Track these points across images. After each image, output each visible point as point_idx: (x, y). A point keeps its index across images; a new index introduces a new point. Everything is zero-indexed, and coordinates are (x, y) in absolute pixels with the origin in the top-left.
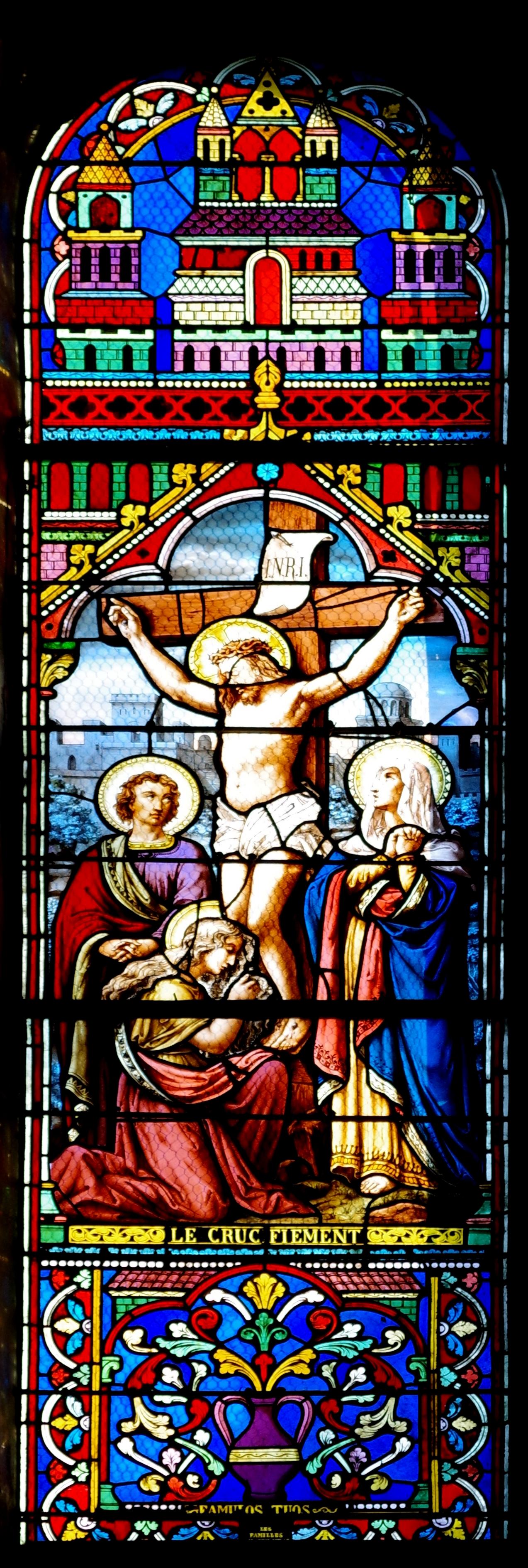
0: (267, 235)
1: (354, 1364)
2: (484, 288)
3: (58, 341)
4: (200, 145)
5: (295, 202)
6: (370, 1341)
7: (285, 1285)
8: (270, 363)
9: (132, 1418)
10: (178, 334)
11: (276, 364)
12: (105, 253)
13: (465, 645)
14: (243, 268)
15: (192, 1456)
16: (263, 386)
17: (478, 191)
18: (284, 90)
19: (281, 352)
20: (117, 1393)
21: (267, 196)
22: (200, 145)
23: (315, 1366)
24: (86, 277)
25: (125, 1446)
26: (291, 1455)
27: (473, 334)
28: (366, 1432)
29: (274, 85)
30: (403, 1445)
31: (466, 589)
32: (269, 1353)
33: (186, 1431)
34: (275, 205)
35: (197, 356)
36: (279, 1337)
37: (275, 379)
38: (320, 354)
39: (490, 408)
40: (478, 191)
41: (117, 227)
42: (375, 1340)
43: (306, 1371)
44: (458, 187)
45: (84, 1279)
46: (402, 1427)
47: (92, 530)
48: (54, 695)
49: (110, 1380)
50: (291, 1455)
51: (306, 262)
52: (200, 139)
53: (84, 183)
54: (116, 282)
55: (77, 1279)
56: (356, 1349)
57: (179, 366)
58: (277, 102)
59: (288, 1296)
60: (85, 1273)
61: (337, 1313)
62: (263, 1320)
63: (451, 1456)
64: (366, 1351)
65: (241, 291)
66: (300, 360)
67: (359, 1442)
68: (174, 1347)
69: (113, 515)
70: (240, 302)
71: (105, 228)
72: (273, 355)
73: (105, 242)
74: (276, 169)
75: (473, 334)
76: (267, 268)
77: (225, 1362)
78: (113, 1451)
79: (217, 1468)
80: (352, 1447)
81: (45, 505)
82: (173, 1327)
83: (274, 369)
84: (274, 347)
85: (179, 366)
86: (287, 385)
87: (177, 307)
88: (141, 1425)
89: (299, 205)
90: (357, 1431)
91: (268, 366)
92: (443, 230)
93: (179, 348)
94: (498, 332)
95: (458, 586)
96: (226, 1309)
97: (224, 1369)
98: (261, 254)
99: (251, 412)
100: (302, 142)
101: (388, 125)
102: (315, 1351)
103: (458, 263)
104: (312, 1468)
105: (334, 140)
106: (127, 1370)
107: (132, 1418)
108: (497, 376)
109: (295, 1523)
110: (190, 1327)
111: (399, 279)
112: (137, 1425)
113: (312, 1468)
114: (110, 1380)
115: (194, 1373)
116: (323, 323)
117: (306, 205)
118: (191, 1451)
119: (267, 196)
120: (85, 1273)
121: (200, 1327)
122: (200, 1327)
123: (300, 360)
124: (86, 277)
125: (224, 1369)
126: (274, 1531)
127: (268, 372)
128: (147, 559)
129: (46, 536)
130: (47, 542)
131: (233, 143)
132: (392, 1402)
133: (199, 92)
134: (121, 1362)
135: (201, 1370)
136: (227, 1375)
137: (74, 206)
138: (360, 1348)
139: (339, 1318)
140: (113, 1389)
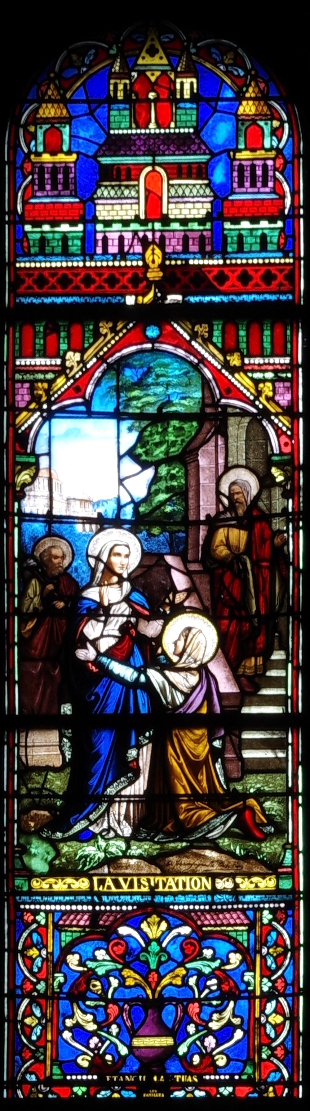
0: (154, 155)
1: (209, 977)
2: (286, 188)
3: (25, 234)
4: (112, 88)
5: (169, 127)
6: (219, 961)
7: (168, 922)
8: (155, 247)
9: (72, 1016)
10: (99, 227)
11: (158, 246)
12: (55, 169)
13: (276, 455)
14: (138, 180)
15: (108, 1042)
16: (151, 265)
17: (285, 117)
18: (162, 44)
19: (162, 238)
20: (64, 999)
21: (152, 125)
22: (112, 88)
23: (185, 979)
24: (42, 188)
25: (67, 1035)
26: (169, 1041)
27: (280, 224)
28: (214, 1026)
29: (156, 39)
30: (239, 1034)
31: (281, 417)
32: (157, 970)
33: (103, 1025)
34: (157, 131)
35: (110, 242)
36: (163, 959)
37: (158, 261)
38: (186, 239)
39: (291, 276)
40: (285, 117)
41: (61, 151)
42: (222, 960)
43: (179, 983)
44: (273, 115)
45: (41, 918)
46: (236, 1021)
47: (45, 372)
48: (24, 496)
49: (58, 990)
50: (169, 1041)
51: (177, 171)
52: (112, 81)
53: (41, 118)
54: (60, 191)
55: (38, 918)
56: (209, 966)
57: (99, 250)
58: (157, 51)
59: (170, 929)
60: (43, 914)
61: (200, 941)
62: (154, 947)
63: (267, 1041)
64: (217, 969)
65: (136, 196)
66: (174, 245)
67: (211, 1032)
68: (97, 967)
69: (59, 361)
70: (136, 203)
71: (53, 153)
72: (157, 241)
73: (54, 163)
74: (159, 104)
75: (280, 224)
76: (153, 178)
77: (128, 977)
78: (60, 1037)
79: (124, 1050)
80: (206, 1036)
81: (17, 354)
82: (97, 953)
83: (157, 251)
84: (158, 235)
85: (99, 250)
86: (167, 263)
87: (98, 208)
88: (77, 1022)
89: (172, 131)
90: (211, 1025)
91: (153, 250)
92: (263, 148)
93: (99, 236)
94: (296, 220)
95: (277, 415)
96: (131, 939)
97: (130, 982)
98: (149, 169)
99: (144, 283)
100: (175, 83)
101: (227, 68)
102: (186, 969)
103: (271, 173)
104: (182, 1049)
105: (194, 80)
106: (70, 982)
107: (72, 1016)
108: (297, 256)
109: (172, 1088)
110: (108, 953)
111: (235, 185)
112: (74, 1022)
113: (182, 1049)
114: (58, 990)
115: (110, 985)
116: (188, 217)
117: (177, 131)
118: (107, 1039)
119: (152, 125)
120: (43, 914)
121: (114, 952)
122: (114, 952)
123: (174, 245)
124: (42, 188)
125: (130, 982)
126: (158, 1092)
127: (153, 254)
128: (80, 394)
129: (18, 376)
130: (19, 381)
131: (131, 83)
132: (232, 1004)
133: (111, 48)
134: (65, 976)
135: (114, 982)
136: (130, 987)
137: (34, 136)
138: (213, 967)
139: (200, 945)
140: (62, 996)
